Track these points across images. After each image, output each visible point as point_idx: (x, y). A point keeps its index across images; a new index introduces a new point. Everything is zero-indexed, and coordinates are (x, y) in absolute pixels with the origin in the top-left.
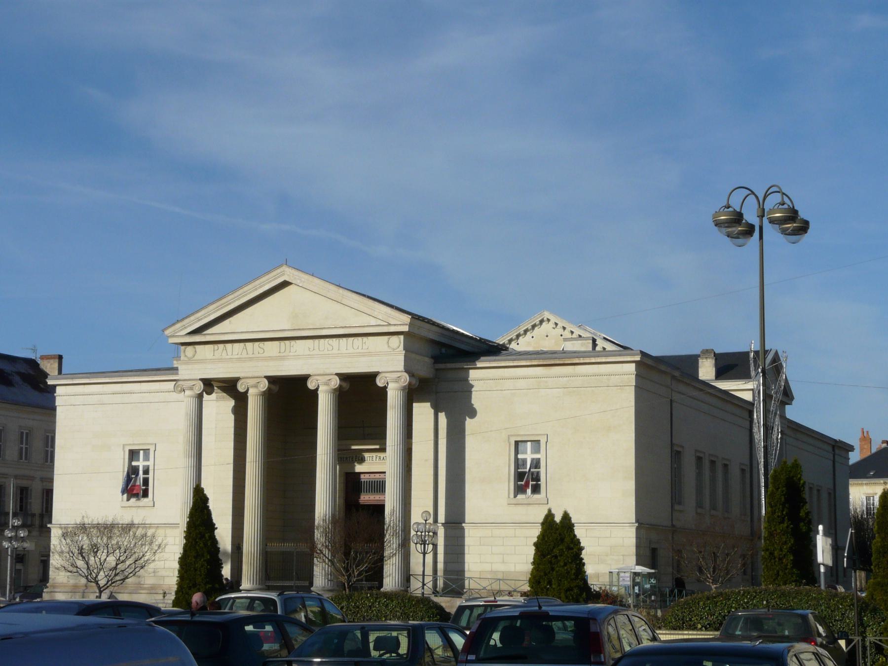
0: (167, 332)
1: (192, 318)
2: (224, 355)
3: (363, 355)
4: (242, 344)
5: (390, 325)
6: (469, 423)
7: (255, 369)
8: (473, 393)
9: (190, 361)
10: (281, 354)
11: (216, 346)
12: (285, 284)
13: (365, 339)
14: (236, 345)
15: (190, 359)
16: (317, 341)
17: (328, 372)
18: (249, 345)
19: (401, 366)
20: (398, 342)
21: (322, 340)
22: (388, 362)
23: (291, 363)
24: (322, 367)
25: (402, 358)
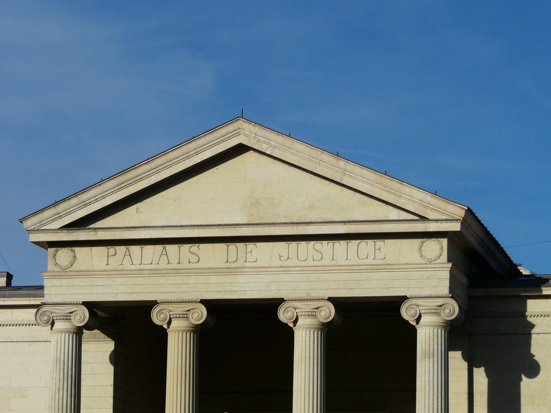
0: (29, 223)
1: (74, 201)
2: (127, 264)
3: (377, 268)
4: (159, 247)
5: (423, 218)
6: (527, 385)
7: (181, 290)
8: (534, 336)
9: (65, 273)
10: (229, 265)
11: (112, 250)
12: (240, 149)
13: (379, 243)
14: (149, 249)
15: (64, 269)
16: (294, 244)
17: (314, 295)
18: (172, 249)
19: (444, 288)
20: (438, 249)
21: (303, 244)
22: (421, 282)
23: (250, 278)
24: (305, 286)
25: (446, 275)
